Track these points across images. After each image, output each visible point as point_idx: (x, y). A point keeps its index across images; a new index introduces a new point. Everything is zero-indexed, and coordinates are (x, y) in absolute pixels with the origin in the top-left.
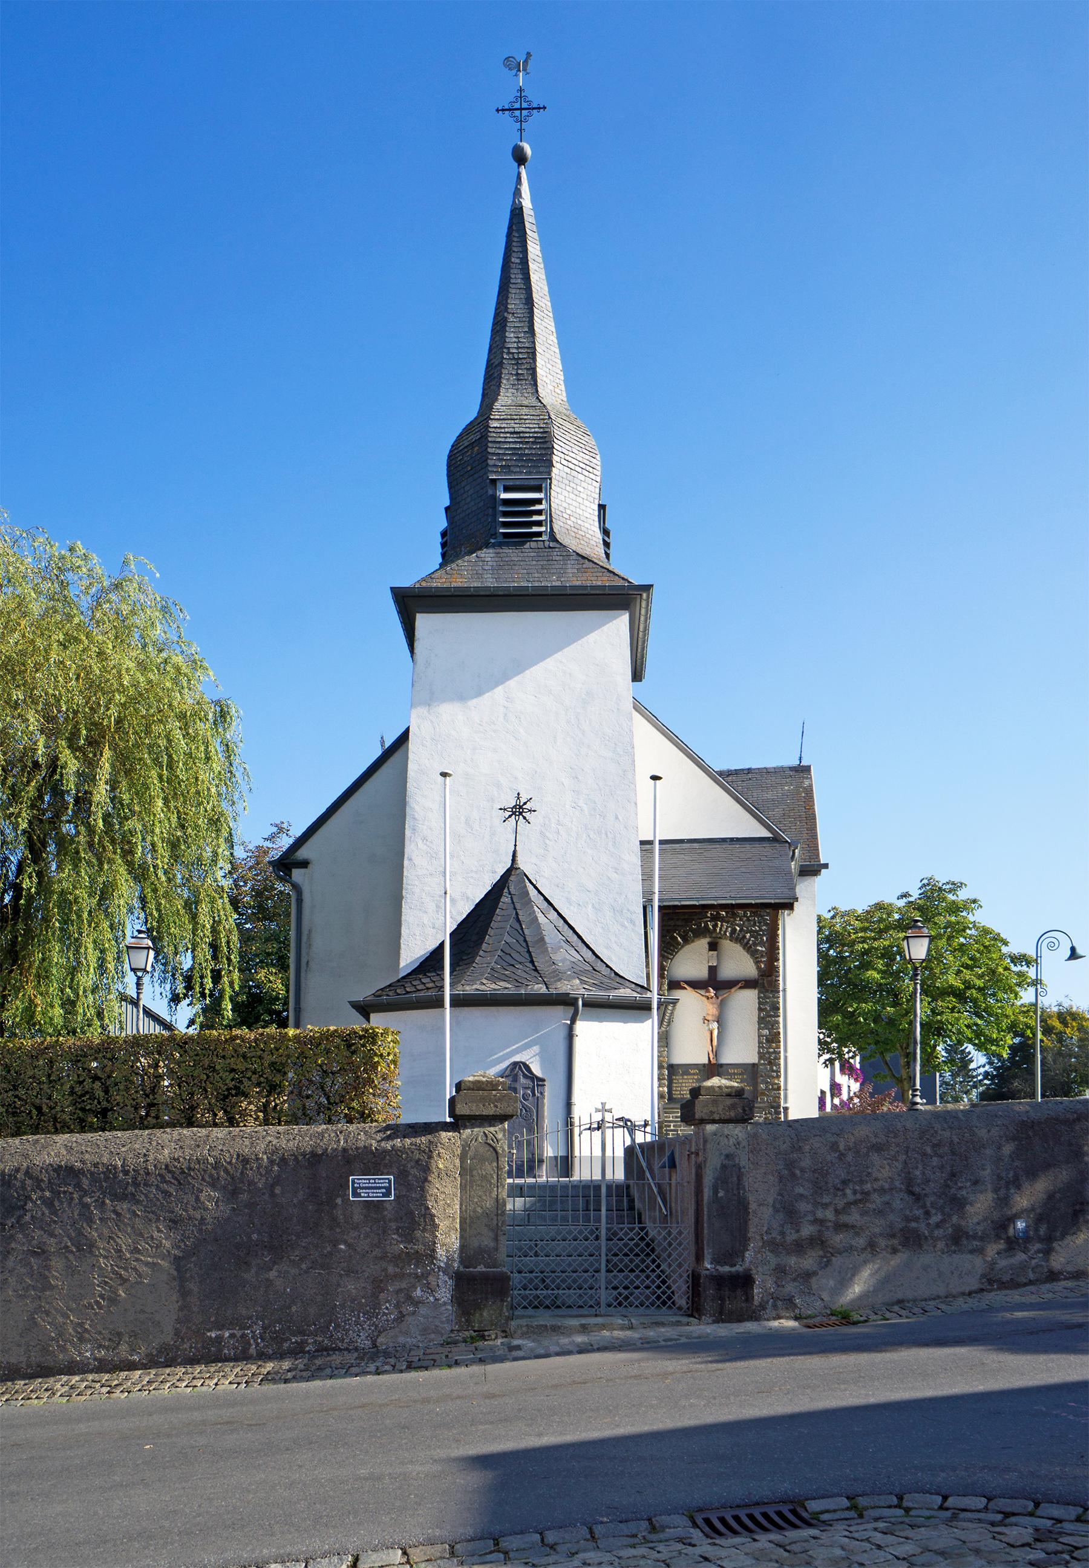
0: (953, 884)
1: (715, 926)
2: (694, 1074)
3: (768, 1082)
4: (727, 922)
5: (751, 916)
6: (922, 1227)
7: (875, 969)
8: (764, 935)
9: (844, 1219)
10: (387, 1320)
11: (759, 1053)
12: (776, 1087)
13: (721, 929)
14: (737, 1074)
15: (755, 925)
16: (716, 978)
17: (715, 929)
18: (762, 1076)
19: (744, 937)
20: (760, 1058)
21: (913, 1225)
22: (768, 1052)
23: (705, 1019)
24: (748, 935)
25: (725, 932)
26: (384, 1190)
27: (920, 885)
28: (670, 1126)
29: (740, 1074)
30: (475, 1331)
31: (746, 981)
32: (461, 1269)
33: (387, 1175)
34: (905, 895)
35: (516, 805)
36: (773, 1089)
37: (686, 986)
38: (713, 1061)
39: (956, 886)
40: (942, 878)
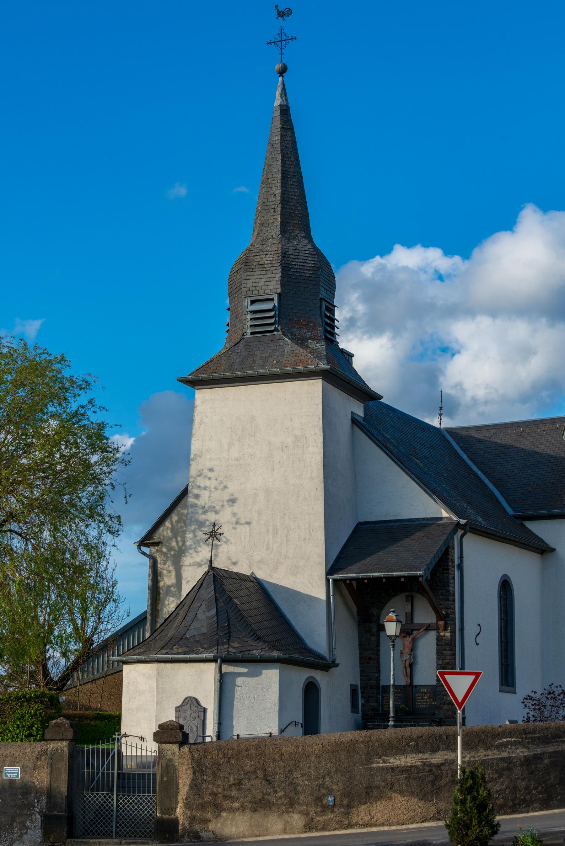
6: (273, 799)
9: (227, 793)
10: (16, 836)
14: (426, 693)
21: (267, 797)
26: (16, 774)
29: (428, 693)
30: (51, 843)
32: (47, 812)
33: (18, 766)
35: (212, 531)
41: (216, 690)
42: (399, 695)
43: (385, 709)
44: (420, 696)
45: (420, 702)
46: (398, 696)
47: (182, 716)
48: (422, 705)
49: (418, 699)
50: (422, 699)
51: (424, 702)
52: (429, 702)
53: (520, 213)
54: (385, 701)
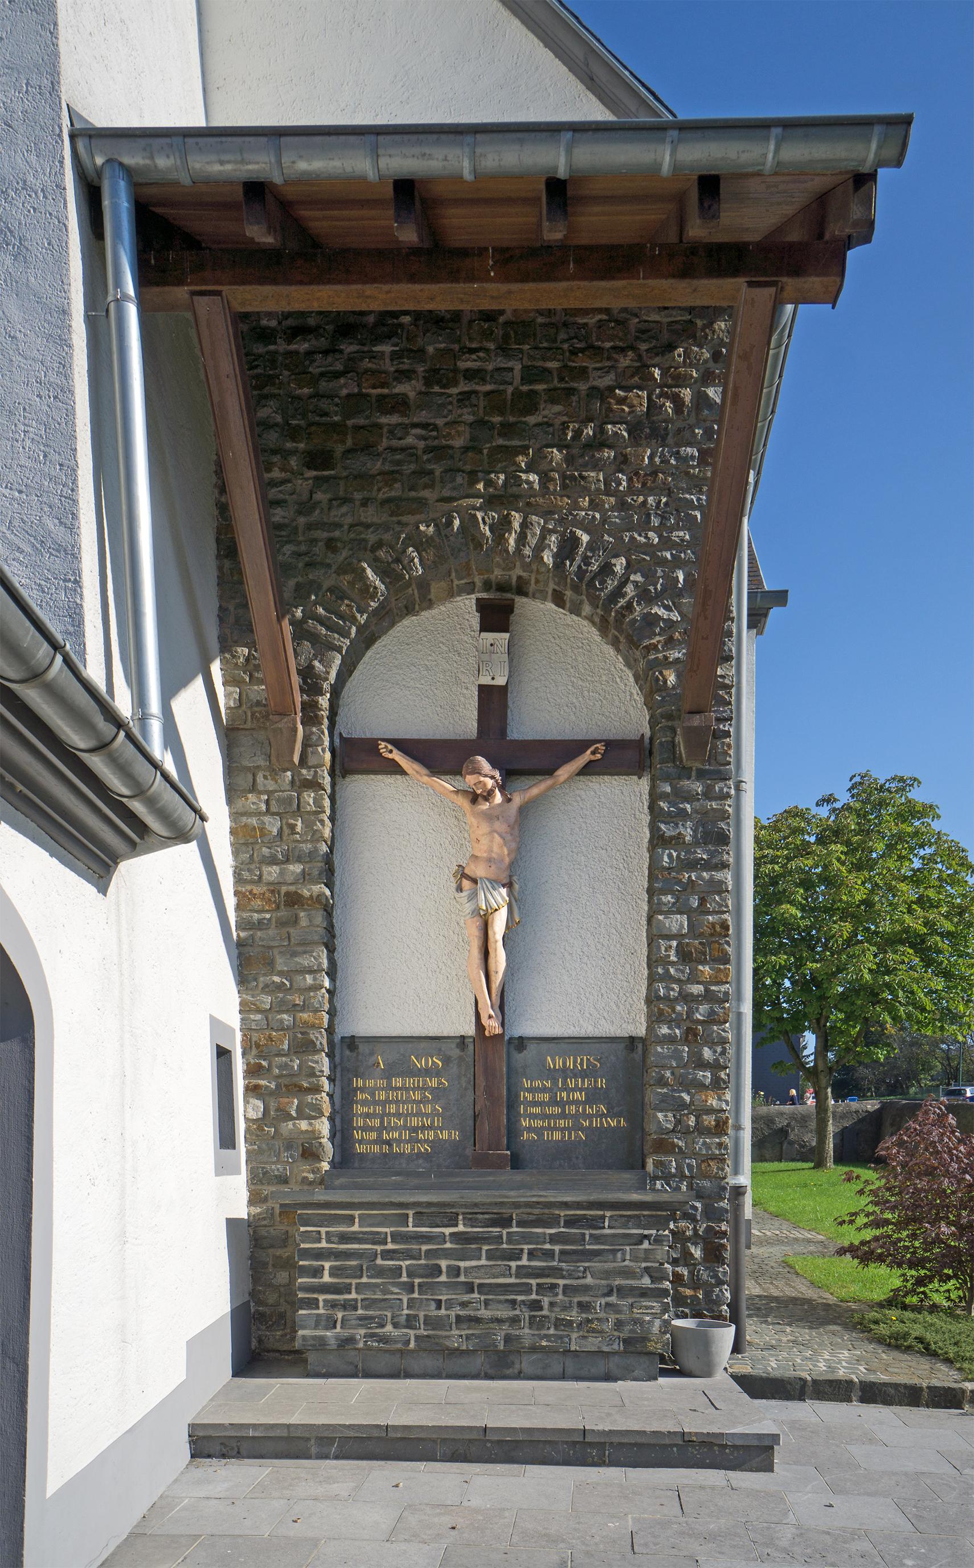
0: (902, 780)
1: (501, 527)
2: (427, 1072)
3: (683, 1105)
4: (547, 514)
5: (631, 490)
7: (792, 903)
8: (677, 563)
11: (652, 999)
12: (709, 1120)
13: (522, 539)
14: (575, 1074)
15: (644, 526)
16: (503, 732)
17: (499, 537)
18: (662, 1082)
19: (607, 569)
20: (655, 1018)
22: (686, 998)
23: (462, 875)
24: (619, 564)
25: (539, 548)
27: (850, 785)
28: (318, 1272)
29: (584, 1074)
31: (612, 745)
34: (828, 800)
36: (701, 1130)
37: (397, 756)
38: (493, 1026)
39: (905, 783)
40: (881, 775)
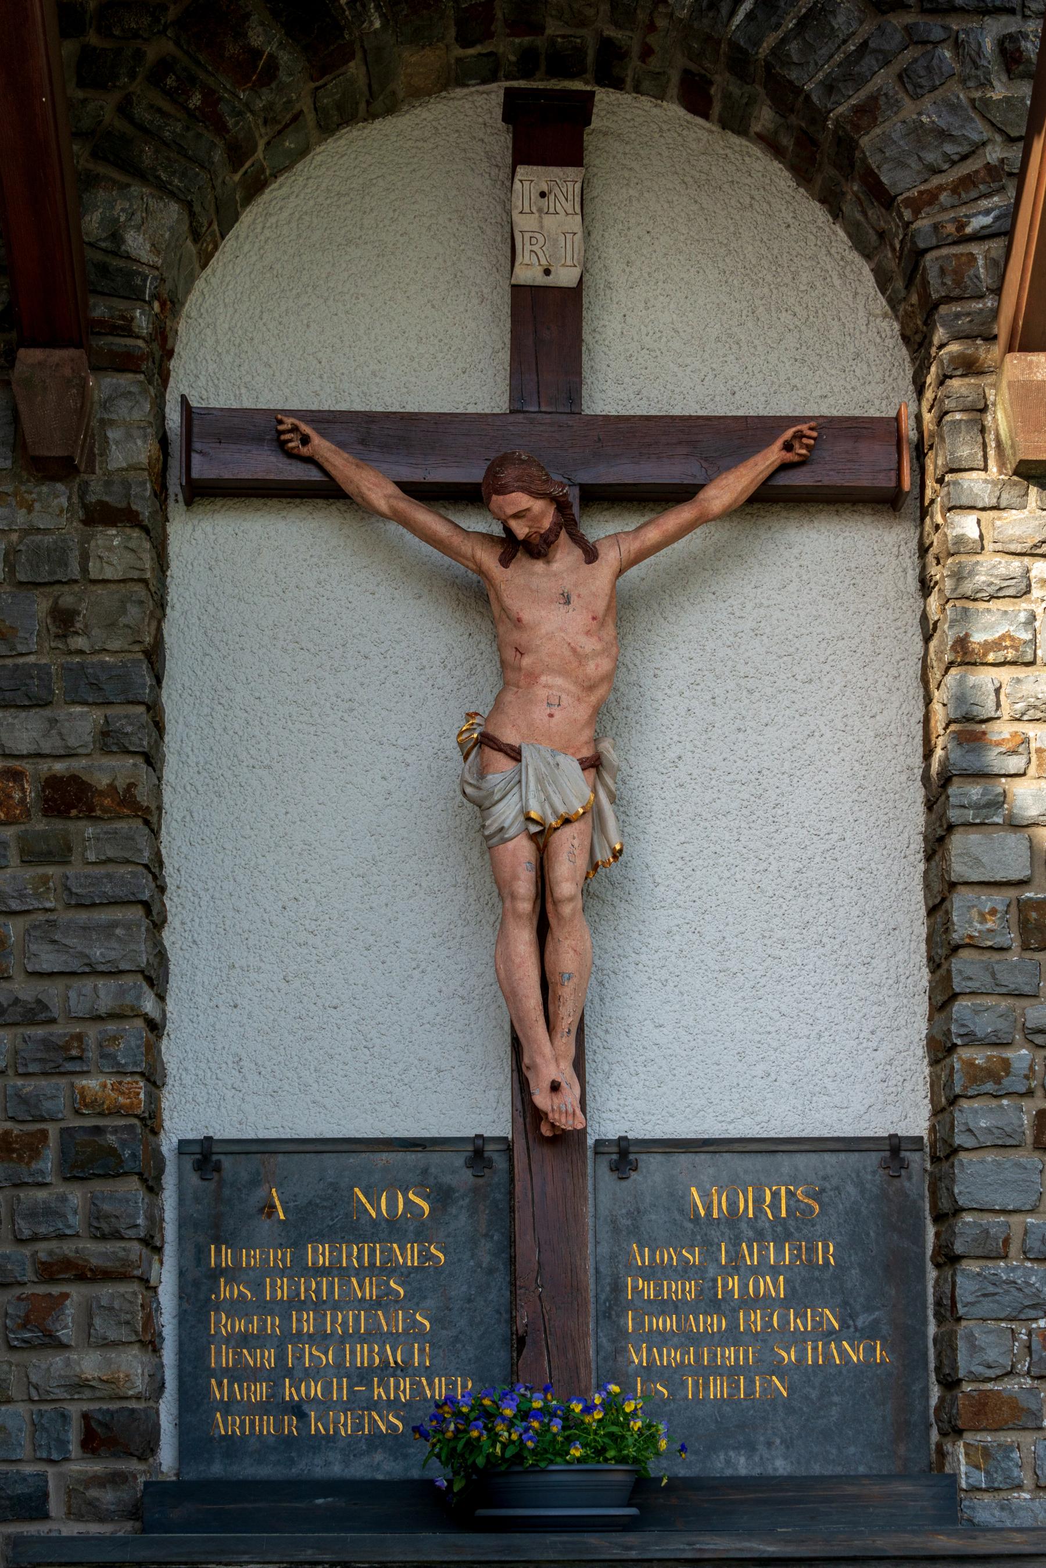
29: (782, 1232)
41: (755, 482)
42: (409, 1256)
43: (224, 1425)
44: (685, 1271)
45: (689, 1339)
46: (406, 1275)
47: (858, 1307)
48: (705, 1372)
49: (663, 1307)
50: (710, 1303)
51: (732, 1337)
52: (798, 1339)
53: (509, 137)
54: (224, 1324)
